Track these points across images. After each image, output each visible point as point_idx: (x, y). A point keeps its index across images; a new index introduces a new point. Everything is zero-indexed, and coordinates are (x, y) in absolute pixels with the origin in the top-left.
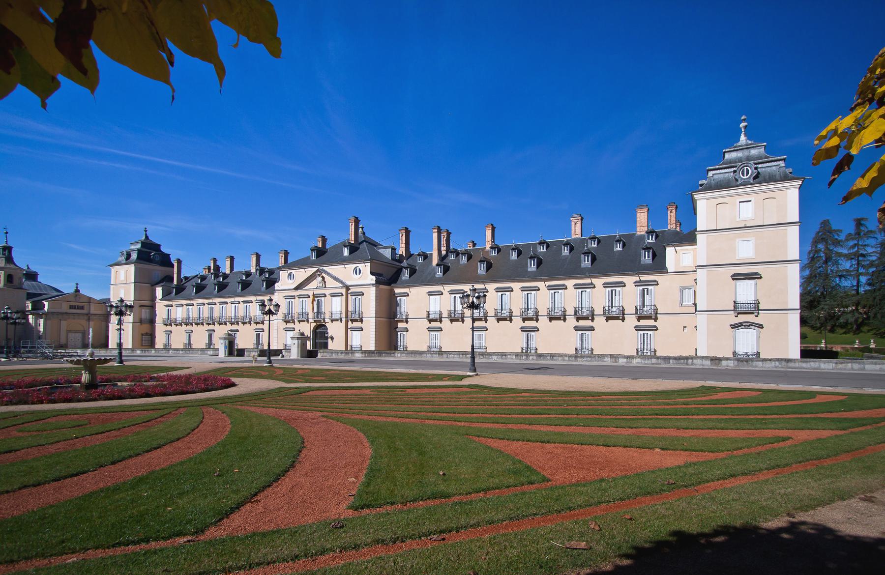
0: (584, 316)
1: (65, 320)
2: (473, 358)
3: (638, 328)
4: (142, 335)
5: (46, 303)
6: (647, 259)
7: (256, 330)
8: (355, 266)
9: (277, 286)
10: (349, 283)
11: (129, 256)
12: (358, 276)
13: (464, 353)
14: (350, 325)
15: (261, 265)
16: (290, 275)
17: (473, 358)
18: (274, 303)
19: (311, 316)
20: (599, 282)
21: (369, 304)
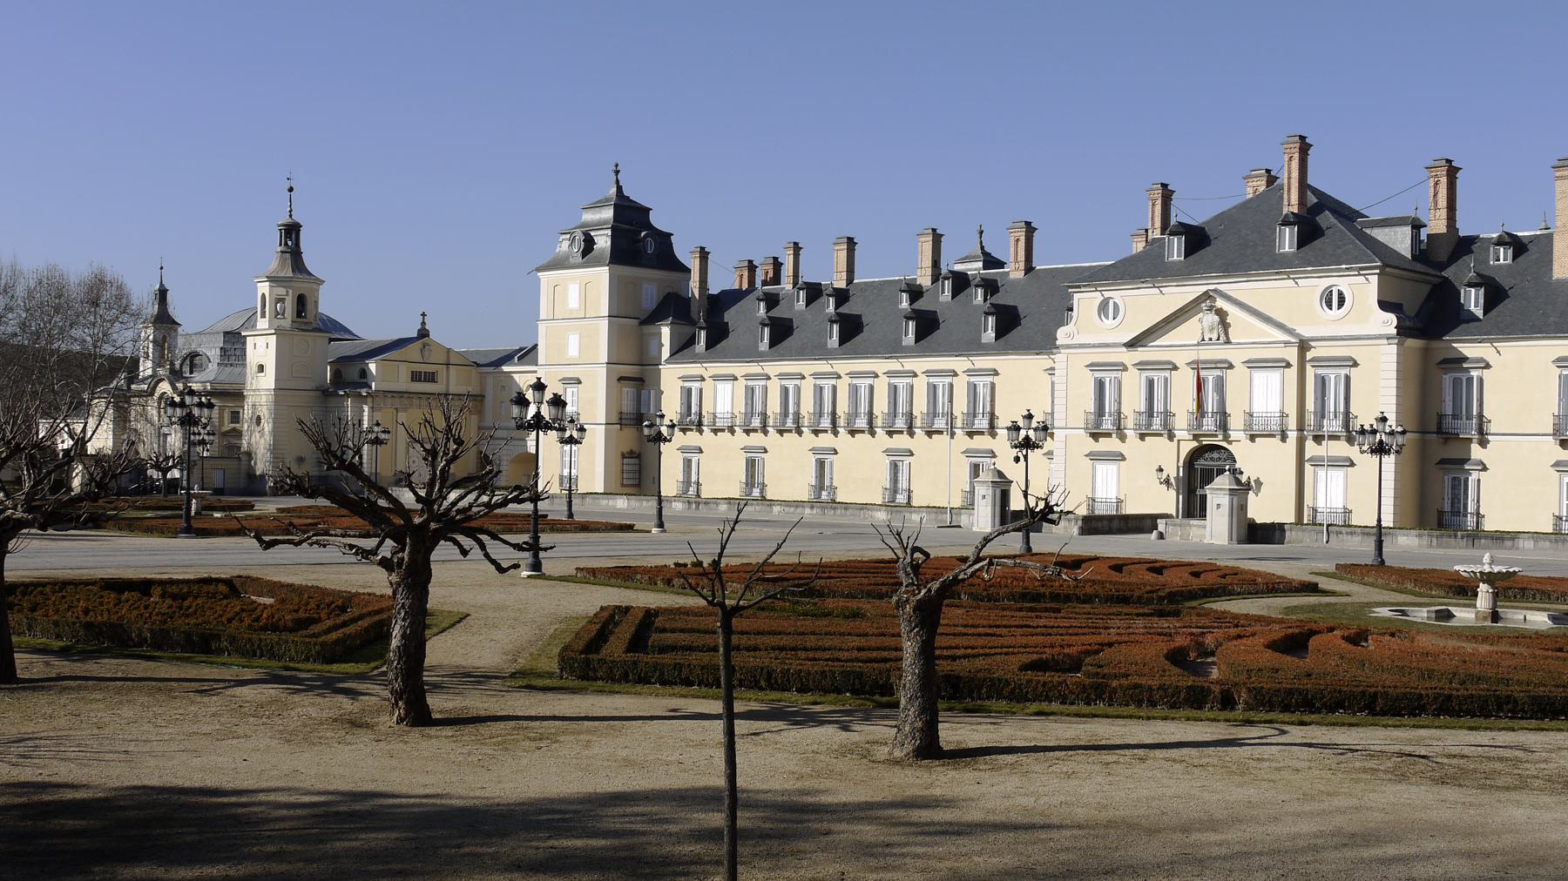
1: (405, 410)
2: (570, 503)
4: (623, 456)
5: (372, 367)
8: (1325, 283)
10: (1306, 332)
11: (589, 243)
12: (1110, 322)
14: (1311, 449)
16: (1103, 307)
17: (570, 503)
18: (548, 395)
19: (1181, 422)
21: (1378, 389)
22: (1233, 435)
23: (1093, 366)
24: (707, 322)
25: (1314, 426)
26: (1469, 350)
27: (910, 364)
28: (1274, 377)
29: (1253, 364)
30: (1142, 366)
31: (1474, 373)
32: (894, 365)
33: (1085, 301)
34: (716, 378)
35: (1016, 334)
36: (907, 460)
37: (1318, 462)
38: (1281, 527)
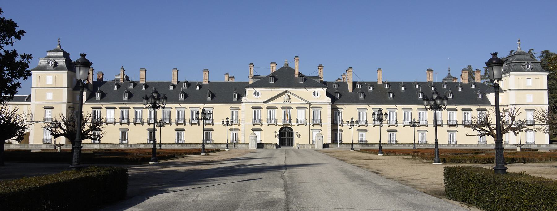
6: (235, 97)
9: (243, 99)
10: (310, 101)
13: (433, 144)
16: (255, 93)
20: (459, 107)
22: (293, 124)
23: (253, 107)
24: (99, 90)
25: (315, 123)
26: (339, 106)
27: (183, 105)
28: (303, 111)
29: (298, 108)
30: (268, 108)
31: (340, 111)
32: (178, 106)
33: (250, 92)
34: (107, 108)
35: (132, 98)
36: (183, 132)
37: (313, 130)
38: (328, 144)
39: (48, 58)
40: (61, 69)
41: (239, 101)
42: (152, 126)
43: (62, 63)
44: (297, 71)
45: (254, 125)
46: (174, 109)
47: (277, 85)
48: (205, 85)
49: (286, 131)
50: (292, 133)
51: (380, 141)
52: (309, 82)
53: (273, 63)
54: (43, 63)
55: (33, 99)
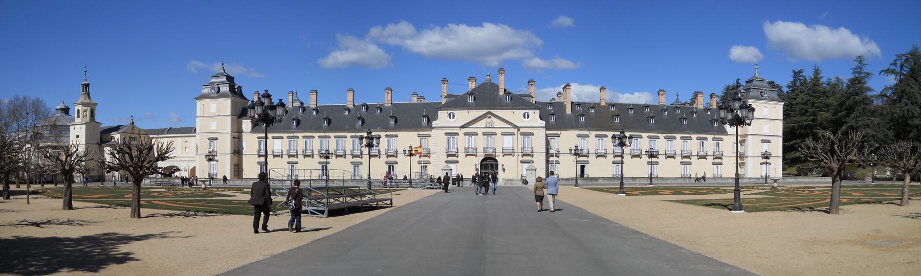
0: (686, 157)
2: (622, 183)
3: (289, 163)
6: (425, 121)
7: (387, 163)
9: (434, 124)
15: (252, 96)
17: (622, 183)
23: (446, 134)
29: (503, 134)
30: (466, 134)
33: (442, 115)
39: (211, 84)
40: (224, 96)
41: (429, 127)
42: (263, 159)
43: (225, 89)
44: (502, 86)
45: (449, 156)
46: (316, 138)
47: (477, 107)
48: (388, 107)
49: (489, 162)
50: (497, 166)
51: (369, 178)
52: (520, 102)
53: (471, 78)
54: (206, 90)
55: (197, 131)
